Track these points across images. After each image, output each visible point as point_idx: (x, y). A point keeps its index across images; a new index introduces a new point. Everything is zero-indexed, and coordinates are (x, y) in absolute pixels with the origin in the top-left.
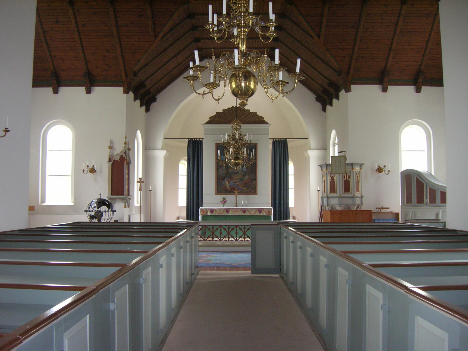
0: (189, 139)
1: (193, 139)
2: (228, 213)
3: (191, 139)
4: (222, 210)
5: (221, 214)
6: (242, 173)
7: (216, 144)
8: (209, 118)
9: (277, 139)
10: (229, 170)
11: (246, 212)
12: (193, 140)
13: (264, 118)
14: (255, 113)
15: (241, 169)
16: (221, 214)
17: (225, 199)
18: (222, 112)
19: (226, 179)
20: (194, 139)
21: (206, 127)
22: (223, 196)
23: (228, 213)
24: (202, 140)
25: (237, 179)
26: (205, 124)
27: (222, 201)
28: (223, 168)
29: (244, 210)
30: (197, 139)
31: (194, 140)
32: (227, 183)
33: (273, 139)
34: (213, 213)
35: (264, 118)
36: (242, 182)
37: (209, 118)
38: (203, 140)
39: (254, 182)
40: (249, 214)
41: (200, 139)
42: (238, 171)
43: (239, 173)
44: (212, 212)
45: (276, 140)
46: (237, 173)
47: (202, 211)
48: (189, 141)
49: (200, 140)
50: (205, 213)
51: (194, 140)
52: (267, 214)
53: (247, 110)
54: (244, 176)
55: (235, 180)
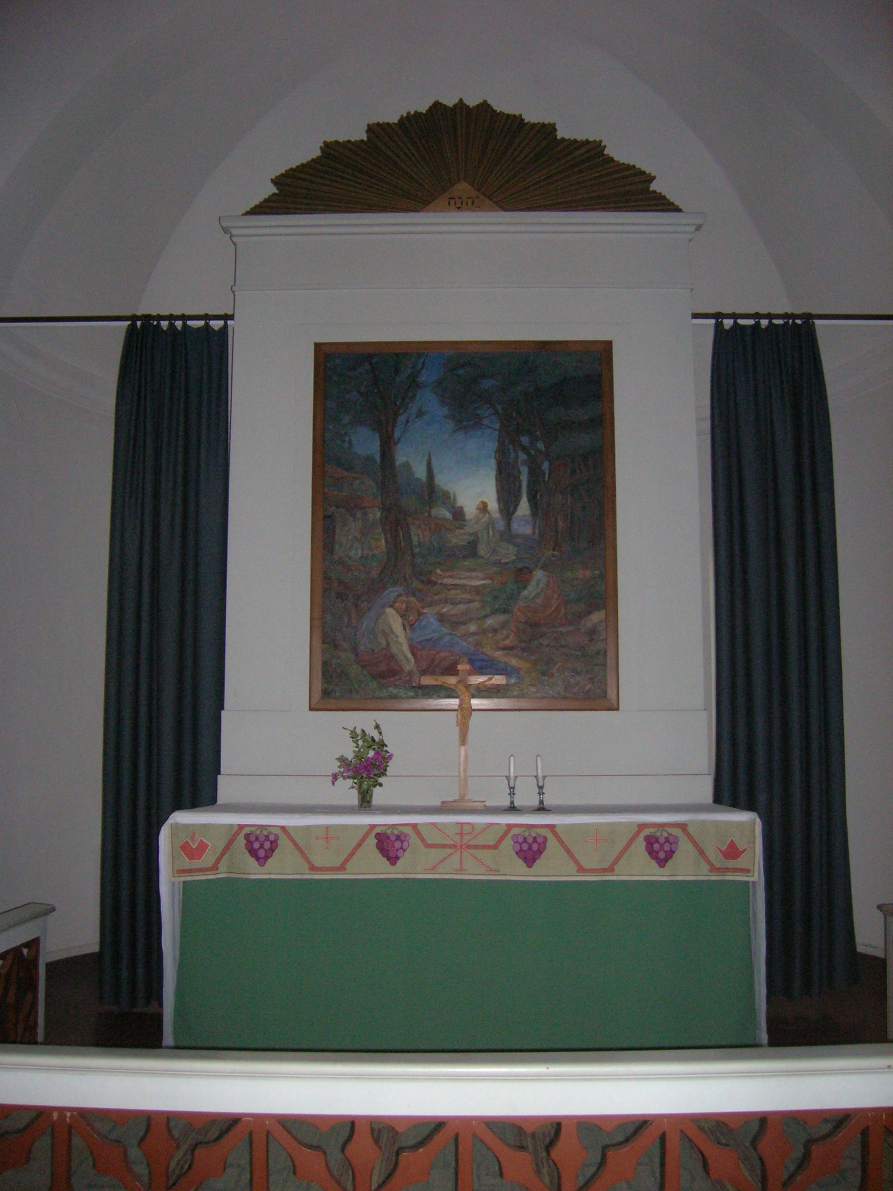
0: (134, 318)
1: (160, 318)
2: (393, 860)
3: (147, 318)
4: (216, 845)
5: (611, 869)
6: (508, 553)
7: (318, 346)
8: (276, 182)
9: (217, 317)
10: (413, 531)
11: (540, 852)
12: (164, 324)
13: (651, 179)
14: (587, 142)
15: (501, 525)
16: (342, 868)
17: (371, 743)
18: (365, 139)
19: (392, 592)
20: (171, 318)
21: (609, 224)
22: (364, 720)
23: (393, 860)
24: (226, 326)
25: (466, 596)
26: (248, 213)
27: (350, 756)
28: (371, 516)
29: (662, 835)
30: (189, 323)
31: (172, 326)
32: (394, 620)
33: (718, 316)
34: (670, 863)
35: (651, 179)
36: (502, 618)
37: (276, 182)
38: (230, 322)
39: (597, 617)
40: (573, 867)
41: (207, 317)
42: (475, 534)
43: (482, 550)
44: (662, 855)
45: (185, 326)
46: (471, 549)
47: (185, 847)
48: (131, 332)
49: (207, 324)
50: (208, 859)
51: (172, 326)
52: (713, 869)
53: (535, 125)
54: (522, 575)
55: (454, 603)
